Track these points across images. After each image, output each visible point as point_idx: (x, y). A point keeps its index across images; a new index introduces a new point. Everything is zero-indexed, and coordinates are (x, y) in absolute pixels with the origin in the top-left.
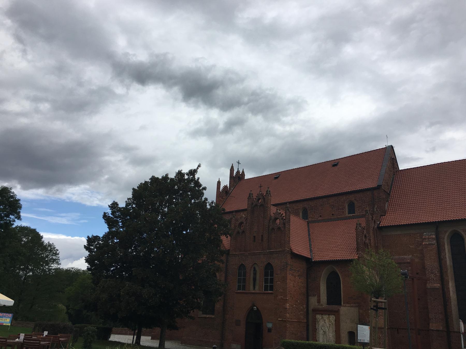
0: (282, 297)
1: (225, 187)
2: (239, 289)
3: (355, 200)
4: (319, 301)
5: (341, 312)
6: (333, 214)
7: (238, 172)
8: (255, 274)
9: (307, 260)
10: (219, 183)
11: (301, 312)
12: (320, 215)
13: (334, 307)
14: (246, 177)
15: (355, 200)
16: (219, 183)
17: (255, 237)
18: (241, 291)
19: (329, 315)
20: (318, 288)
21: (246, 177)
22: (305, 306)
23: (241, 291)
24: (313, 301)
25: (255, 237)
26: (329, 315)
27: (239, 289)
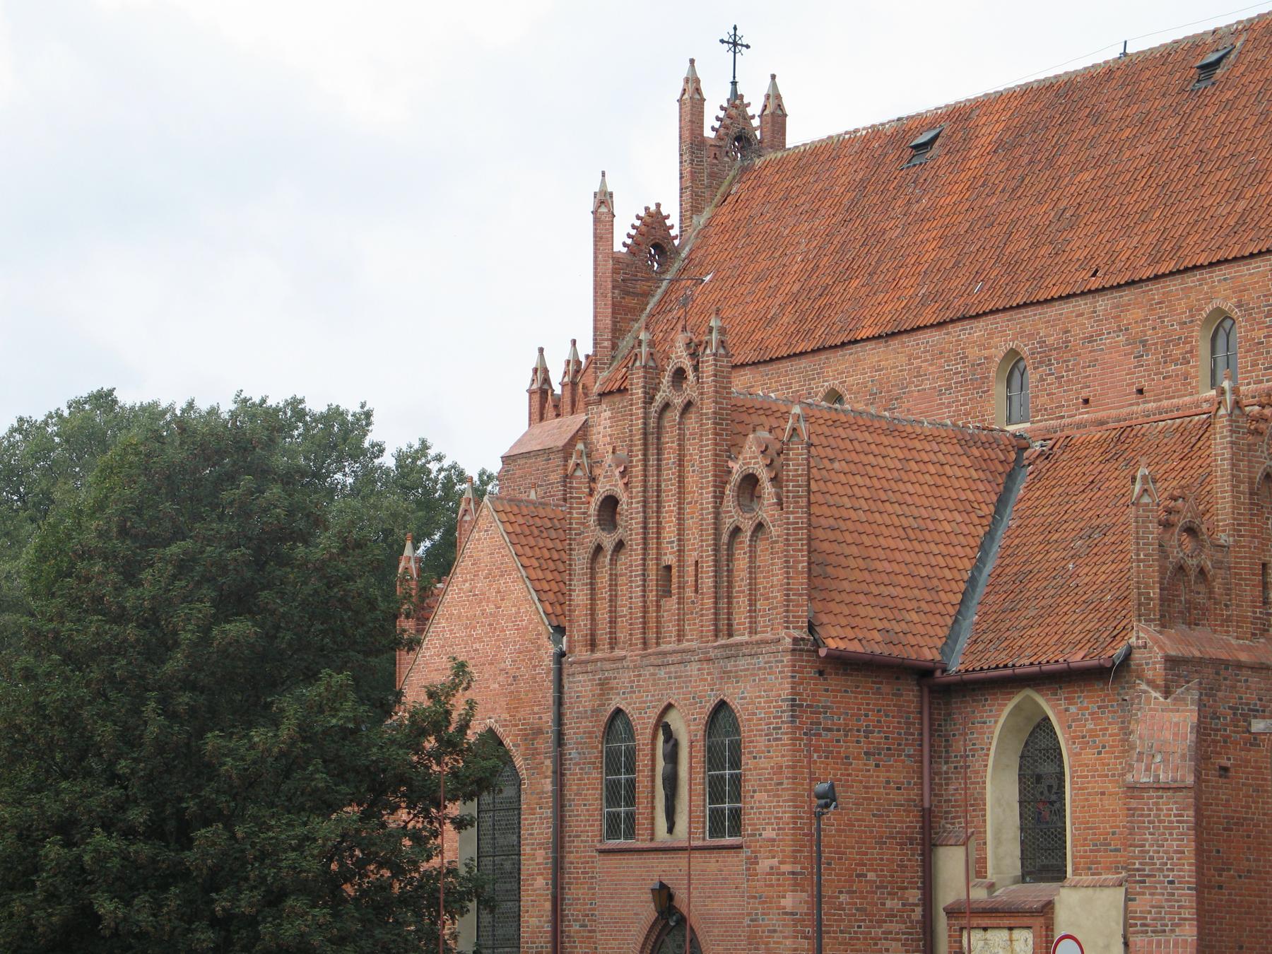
0: (775, 861)
1: (653, 222)
2: (613, 832)
3: (1239, 305)
4: (977, 869)
5: (1064, 921)
6: (1086, 401)
7: (736, 102)
8: (672, 758)
9: (923, 674)
10: (604, 200)
11: (895, 927)
12: (1085, 393)
13: (1036, 892)
14: (798, 135)
15: (1239, 305)
16: (604, 200)
17: (669, 568)
18: (621, 843)
19: (1011, 929)
20: (978, 804)
21: (798, 135)
22: (914, 895)
23: (621, 843)
24: (951, 865)
25: (669, 568)
26: (1011, 929)
27: (613, 832)
